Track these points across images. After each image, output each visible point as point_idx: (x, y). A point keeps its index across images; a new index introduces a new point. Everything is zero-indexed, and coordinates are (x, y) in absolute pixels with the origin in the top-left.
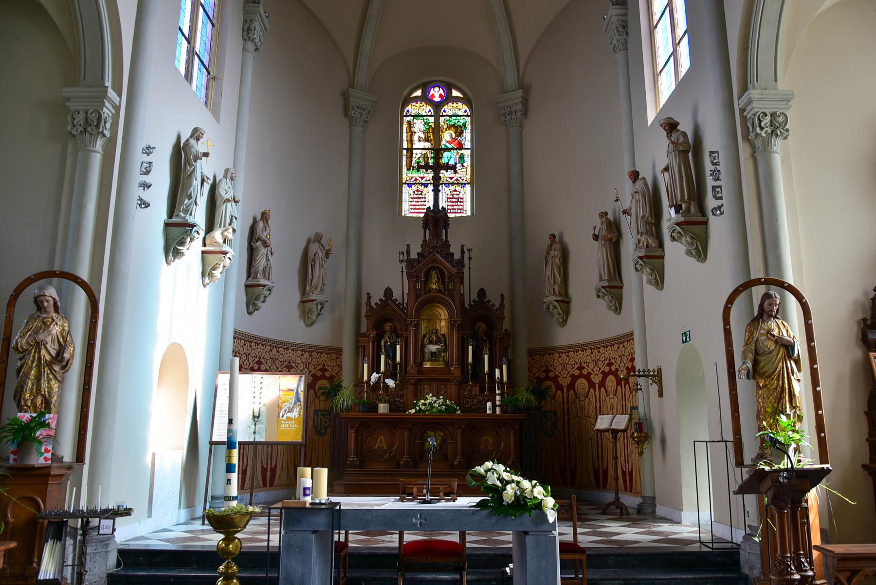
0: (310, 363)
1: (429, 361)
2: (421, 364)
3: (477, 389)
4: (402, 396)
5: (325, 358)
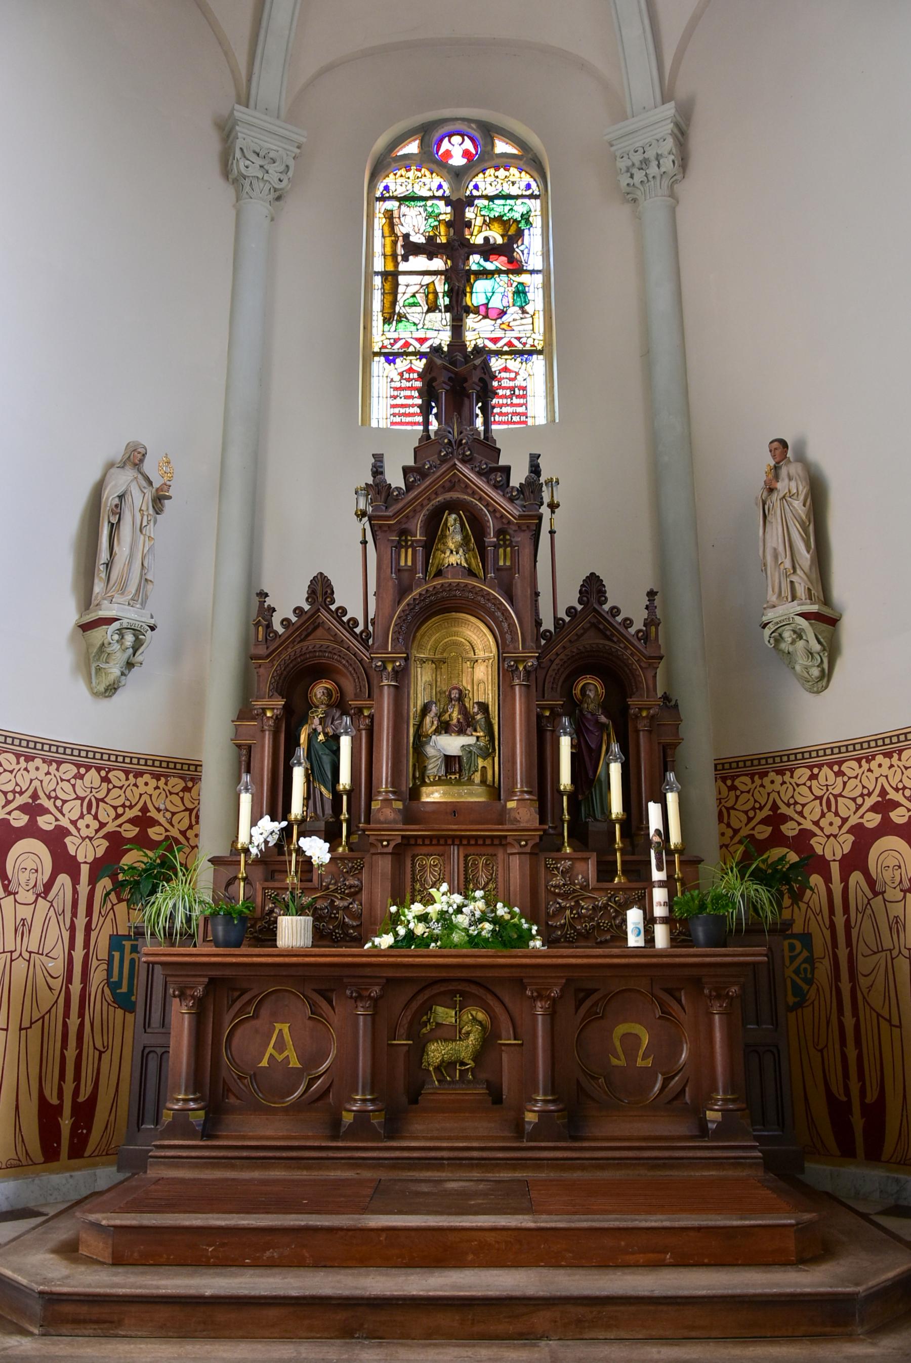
0: (102, 800)
1: (439, 782)
2: (415, 794)
3: (591, 868)
4: (356, 893)
5: (150, 789)
